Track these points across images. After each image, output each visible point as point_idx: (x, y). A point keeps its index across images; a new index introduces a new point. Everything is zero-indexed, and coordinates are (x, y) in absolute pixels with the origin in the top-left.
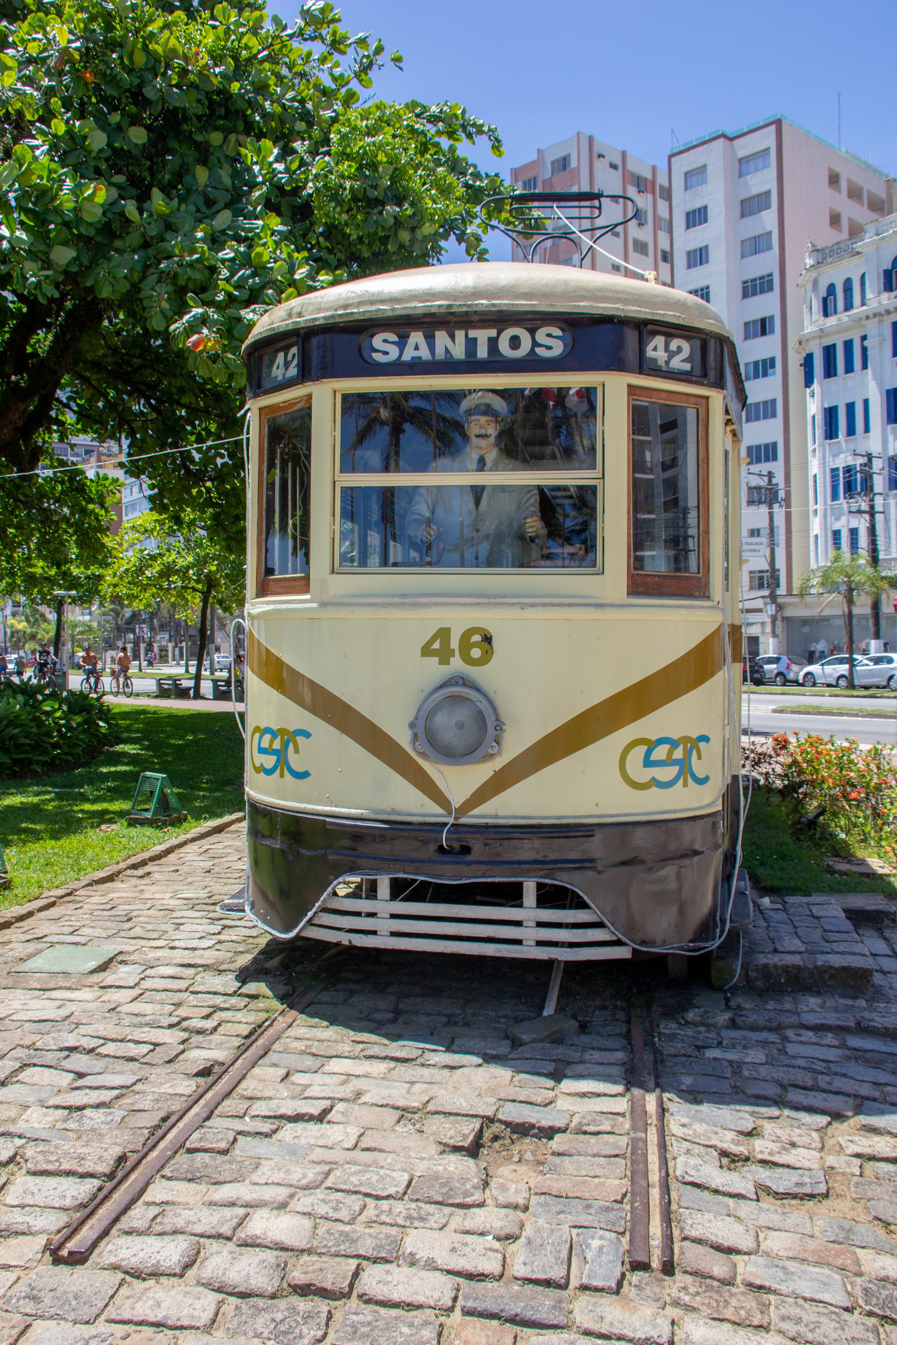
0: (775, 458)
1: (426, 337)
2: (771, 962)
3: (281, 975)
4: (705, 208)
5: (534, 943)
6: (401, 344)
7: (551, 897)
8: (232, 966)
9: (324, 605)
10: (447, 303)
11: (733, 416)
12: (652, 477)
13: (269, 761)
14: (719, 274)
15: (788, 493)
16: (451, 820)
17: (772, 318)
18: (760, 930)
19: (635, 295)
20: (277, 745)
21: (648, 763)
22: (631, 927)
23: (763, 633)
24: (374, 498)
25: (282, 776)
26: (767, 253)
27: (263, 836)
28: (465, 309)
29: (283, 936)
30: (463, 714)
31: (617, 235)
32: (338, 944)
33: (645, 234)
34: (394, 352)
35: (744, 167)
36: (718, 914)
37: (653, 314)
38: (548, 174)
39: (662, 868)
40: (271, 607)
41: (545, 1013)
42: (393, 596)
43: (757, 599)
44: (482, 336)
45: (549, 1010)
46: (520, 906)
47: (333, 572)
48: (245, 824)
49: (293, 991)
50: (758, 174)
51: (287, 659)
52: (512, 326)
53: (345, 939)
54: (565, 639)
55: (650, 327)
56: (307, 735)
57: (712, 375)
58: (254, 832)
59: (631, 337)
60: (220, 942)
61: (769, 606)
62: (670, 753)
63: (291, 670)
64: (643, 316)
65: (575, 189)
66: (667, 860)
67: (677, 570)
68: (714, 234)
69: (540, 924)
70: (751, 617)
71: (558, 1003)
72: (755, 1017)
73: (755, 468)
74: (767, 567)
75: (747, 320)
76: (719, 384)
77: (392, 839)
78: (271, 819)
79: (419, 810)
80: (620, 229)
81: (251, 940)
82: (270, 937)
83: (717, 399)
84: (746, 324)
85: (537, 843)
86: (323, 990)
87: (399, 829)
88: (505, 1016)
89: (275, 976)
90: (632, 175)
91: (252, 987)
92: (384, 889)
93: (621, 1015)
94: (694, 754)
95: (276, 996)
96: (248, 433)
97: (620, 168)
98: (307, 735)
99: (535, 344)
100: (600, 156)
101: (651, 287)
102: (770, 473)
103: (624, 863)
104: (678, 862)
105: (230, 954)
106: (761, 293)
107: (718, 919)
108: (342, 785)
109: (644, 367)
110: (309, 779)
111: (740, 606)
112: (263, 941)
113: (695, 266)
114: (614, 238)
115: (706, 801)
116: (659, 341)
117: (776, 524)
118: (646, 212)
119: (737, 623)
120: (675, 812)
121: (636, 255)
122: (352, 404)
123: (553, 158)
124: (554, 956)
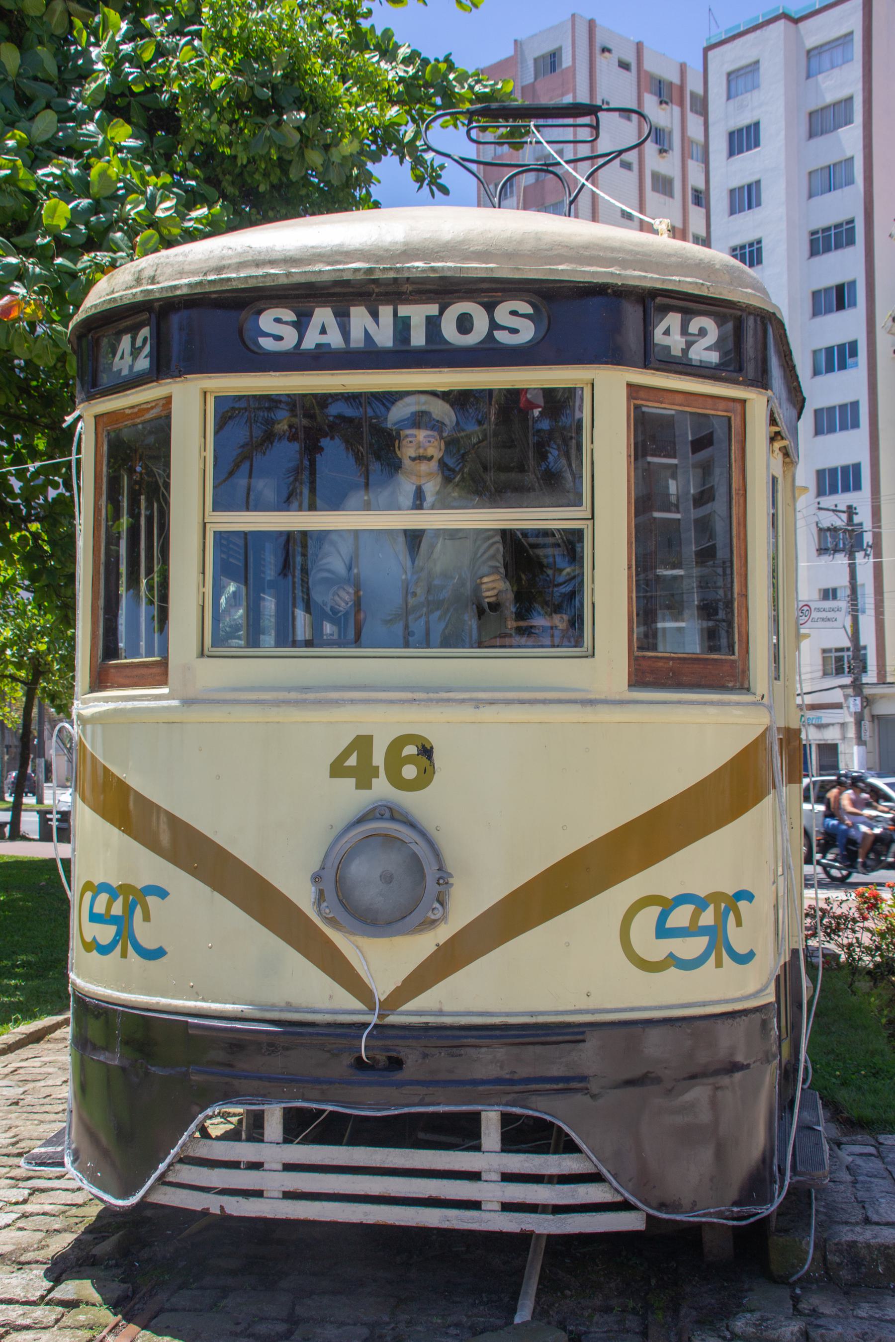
0: (858, 487)
1: (336, 315)
2: (860, 1239)
3: (117, 1265)
4: (757, 125)
5: (498, 1207)
6: (301, 326)
7: (523, 1135)
8: (41, 1255)
9: (188, 702)
10: (366, 265)
11: (783, 427)
12: (678, 516)
13: (106, 933)
14: (775, 223)
15: (877, 537)
16: (373, 1019)
17: (853, 284)
18: (842, 1187)
19: (638, 253)
20: (707, 918)
21: (662, 932)
22: (644, 1181)
23: (844, 738)
24: (269, 546)
25: (124, 955)
26: (847, 189)
27: (95, 1048)
28: (392, 275)
29: (120, 1202)
30: (390, 861)
31: (627, 166)
32: (205, 1213)
33: (669, 166)
34: (290, 336)
35: (814, 62)
36: (776, 1161)
37: (664, 281)
38: (529, 78)
39: (687, 1091)
40: (111, 706)
41: (517, 1320)
42: (290, 689)
43: (835, 689)
44: (418, 314)
45: (523, 1314)
46: (478, 1148)
47: (202, 654)
48: (67, 1032)
49: (135, 1292)
50: (836, 72)
51: (135, 782)
52: (462, 299)
53: (213, 1204)
54: (543, 750)
55: (659, 300)
56: (162, 893)
57: (750, 369)
58: (81, 1043)
59: (632, 314)
60: (25, 1216)
61: (851, 700)
62: (695, 917)
63: (138, 795)
64: (648, 284)
65: (568, 99)
66: (693, 1077)
67: (713, 649)
68: (770, 164)
69: (508, 1177)
70: (827, 716)
71: (537, 1302)
72: (840, 1329)
73: (828, 501)
74: (847, 643)
75: (816, 287)
76: (762, 381)
77: (287, 1049)
78: (107, 1022)
79: (325, 1004)
80: (631, 157)
81: (74, 1211)
82: (101, 1206)
83: (757, 403)
84: (815, 294)
85: (501, 1053)
86: (180, 1288)
87: (297, 1034)
88: (457, 1325)
89: (107, 1267)
90: (651, 77)
91: (69, 1289)
92: (274, 1126)
93: (632, 1322)
94: (731, 918)
95: (106, 1301)
96: (79, 452)
97: (634, 67)
98: (162, 893)
99: (494, 325)
100: (605, 50)
101: (663, 242)
102: (850, 507)
103: (630, 1083)
104: (711, 1080)
105: (39, 1235)
106: (836, 248)
107: (775, 1168)
108: (209, 968)
109: (651, 357)
110: (164, 960)
111: (799, 700)
112: (93, 1211)
113: (741, 210)
114: (624, 171)
115: (751, 988)
116: (673, 320)
117: (860, 580)
118: (670, 133)
119: (794, 725)
120: (704, 1004)
121: (656, 195)
122: (229, 412)
123: (537, 54)
124: (528, 1227)
